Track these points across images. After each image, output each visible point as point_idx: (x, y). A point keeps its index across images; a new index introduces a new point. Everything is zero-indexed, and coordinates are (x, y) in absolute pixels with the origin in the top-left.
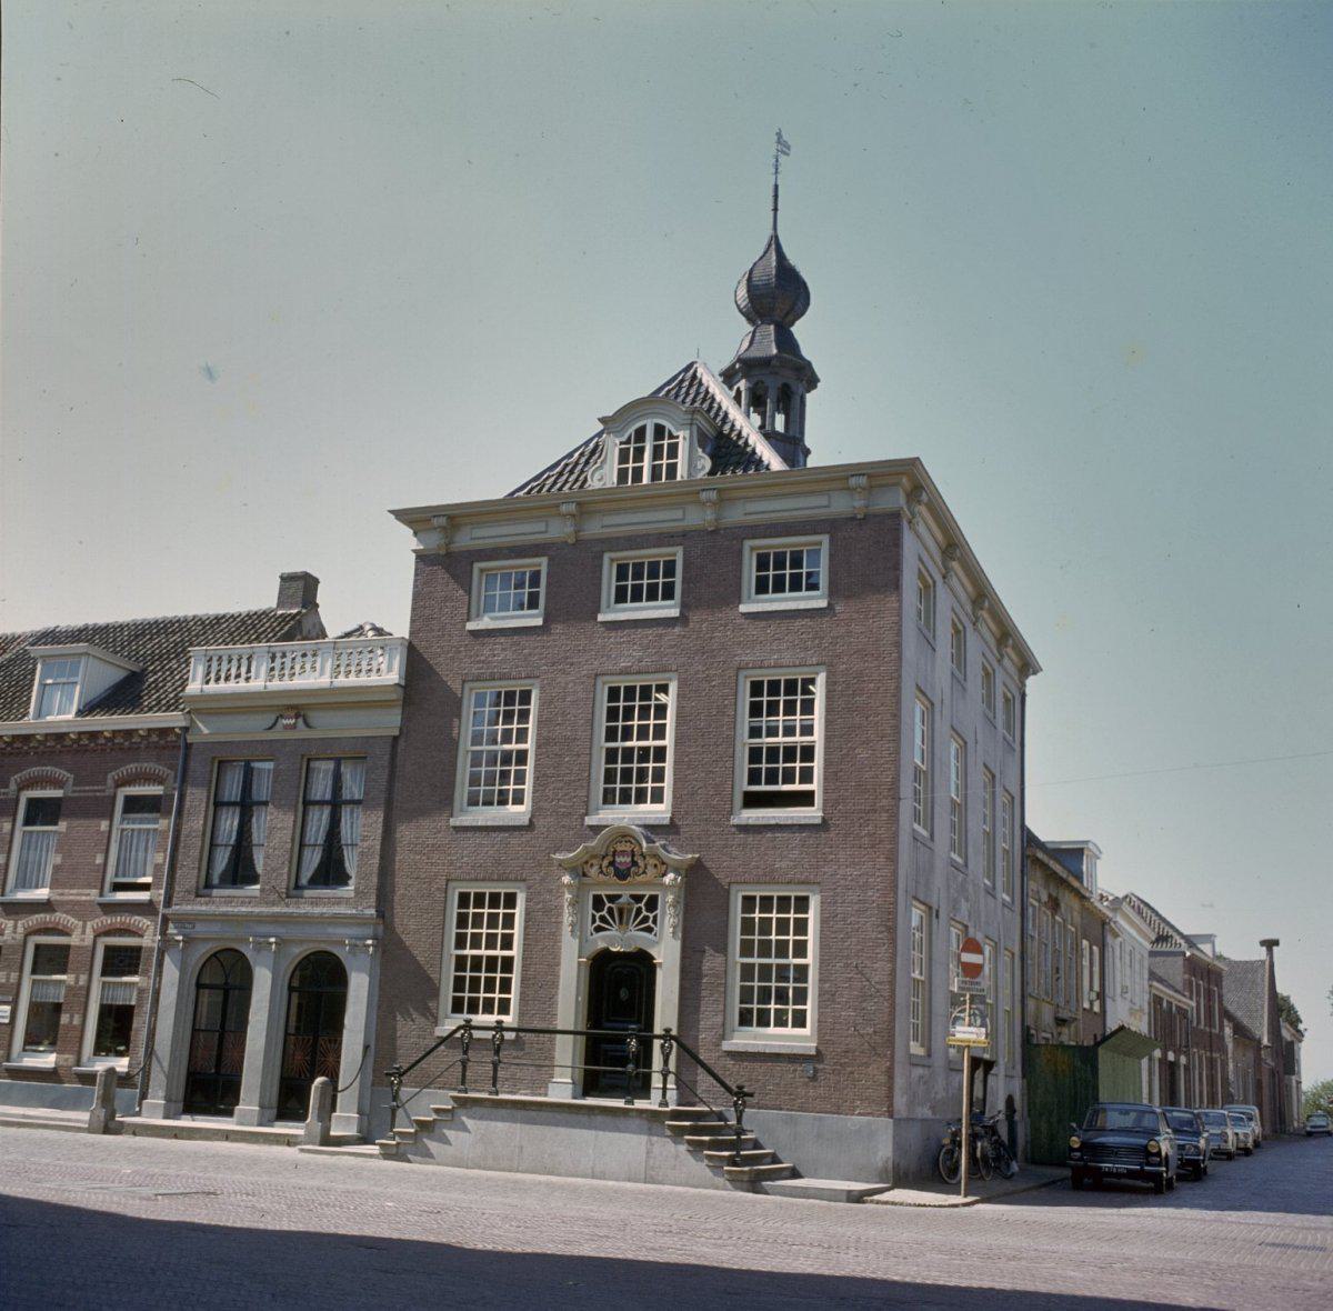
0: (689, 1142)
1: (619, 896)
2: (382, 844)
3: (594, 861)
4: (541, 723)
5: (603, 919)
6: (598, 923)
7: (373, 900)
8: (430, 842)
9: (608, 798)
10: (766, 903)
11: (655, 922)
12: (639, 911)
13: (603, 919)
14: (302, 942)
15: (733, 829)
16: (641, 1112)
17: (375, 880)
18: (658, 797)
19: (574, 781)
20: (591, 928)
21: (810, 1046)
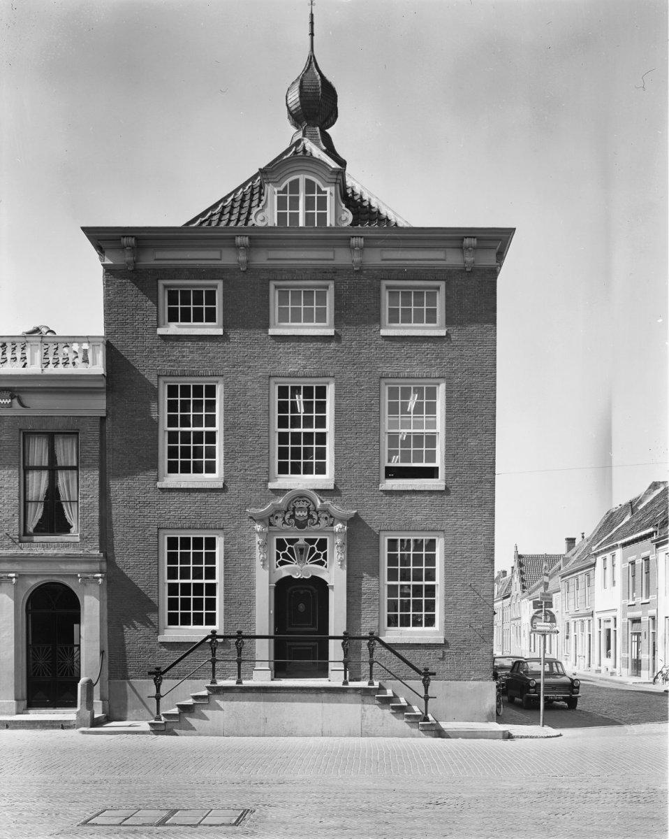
0: (393, 708)
1: (297, 540)
2: (100, 501)
3: (279, 515)
4: (227, 411)
5: (285, 556)
7: (97, 544)
8: (142, 499)
9: (283, 469)
10: (406, 544)
11: (325, 557)
12: (312, 550)
13: (285, 556)
14: (36, 576)
15: (382, 493)
16: (356, 690)
17: (97, 528)
18: (321, 470)
19: (257, 456)
20: (276, 562)
21: (440, 639)
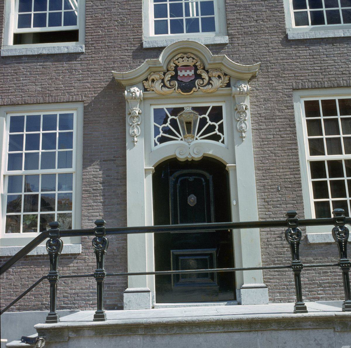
3: (156, 76)
5: (167, 131)
6: (161, 134)
11: (221, 129)
12: (203, 122)
20: (154, 139)
